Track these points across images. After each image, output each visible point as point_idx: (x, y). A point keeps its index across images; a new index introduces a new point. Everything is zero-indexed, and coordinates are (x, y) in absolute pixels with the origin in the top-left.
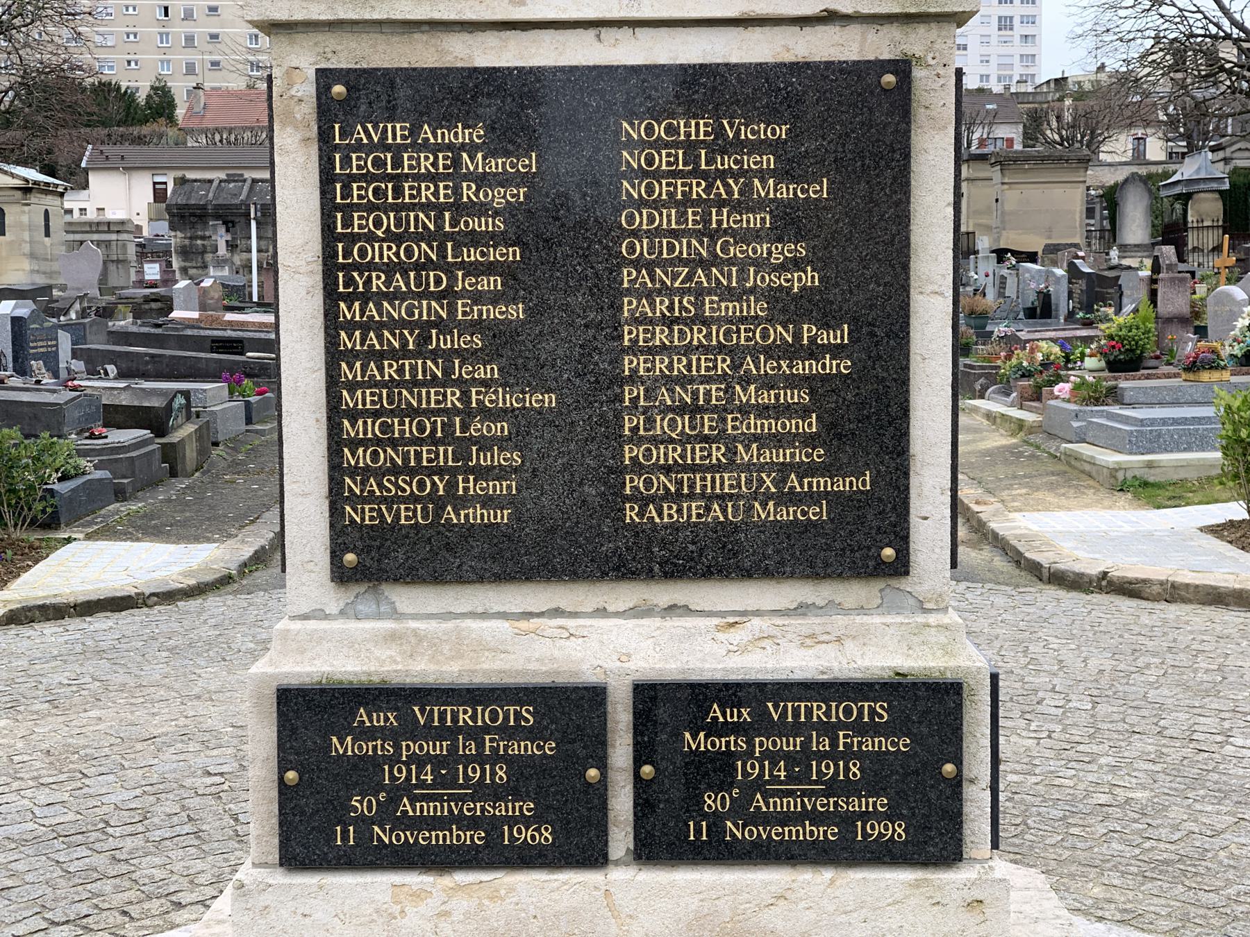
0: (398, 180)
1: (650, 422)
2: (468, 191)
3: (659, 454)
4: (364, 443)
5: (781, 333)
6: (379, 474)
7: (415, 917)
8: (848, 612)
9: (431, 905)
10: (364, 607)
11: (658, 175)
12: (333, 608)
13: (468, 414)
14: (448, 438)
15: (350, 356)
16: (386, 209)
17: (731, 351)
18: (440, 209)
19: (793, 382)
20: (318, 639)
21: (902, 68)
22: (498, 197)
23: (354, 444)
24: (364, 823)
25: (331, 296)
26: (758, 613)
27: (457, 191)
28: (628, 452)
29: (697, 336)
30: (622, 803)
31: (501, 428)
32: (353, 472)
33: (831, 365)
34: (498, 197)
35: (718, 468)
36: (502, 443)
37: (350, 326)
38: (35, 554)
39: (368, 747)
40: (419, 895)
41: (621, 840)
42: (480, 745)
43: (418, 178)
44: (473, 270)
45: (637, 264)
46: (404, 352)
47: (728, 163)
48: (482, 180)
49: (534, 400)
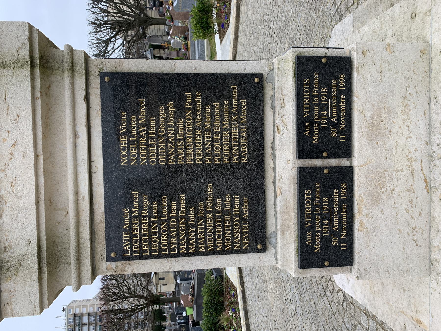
0: (141, 236)
1: (217, 155)
2: (145, 213)
3: (226, 152)
4: (224, 243)
5: (188, 114)
6: (233, 238)
7: (368, 225)
8: (274, 94)
9: (364, 220)
10: (273, 242)
11: (139, 153)
12: (274, 251)
13: (215, 211)
14: (222, 217)
15: (197, 248)
16: (150, 239)
17: (194, 130)
18: (150, 222)
19: (204, 111)
20: (283, 256)
21: (102, 75)
22: (146, 203)
23: (224, 246)
24: (340, 242)
25: (178, 255)
26: (274, 121)
27: (144, 217)
28: (226, 161)
29: (190, 140)
30: (333, 162)
31: (219, 201)
32: (233, 246)
33: (198, 99)
34: (146, 203)
35: (230, 134)
36: (223, 200)
37: (188, 249)
38: (229, 281)
39: (318, 241)
40: (361, 224)
41: (344, 162)
42: (317, 206)
43: (140, 229)
44: (170, 210)
45: (167, 159)
46: (196, 231)
47: (134, 131)
48: (141, 208)
49: (210, 191)
